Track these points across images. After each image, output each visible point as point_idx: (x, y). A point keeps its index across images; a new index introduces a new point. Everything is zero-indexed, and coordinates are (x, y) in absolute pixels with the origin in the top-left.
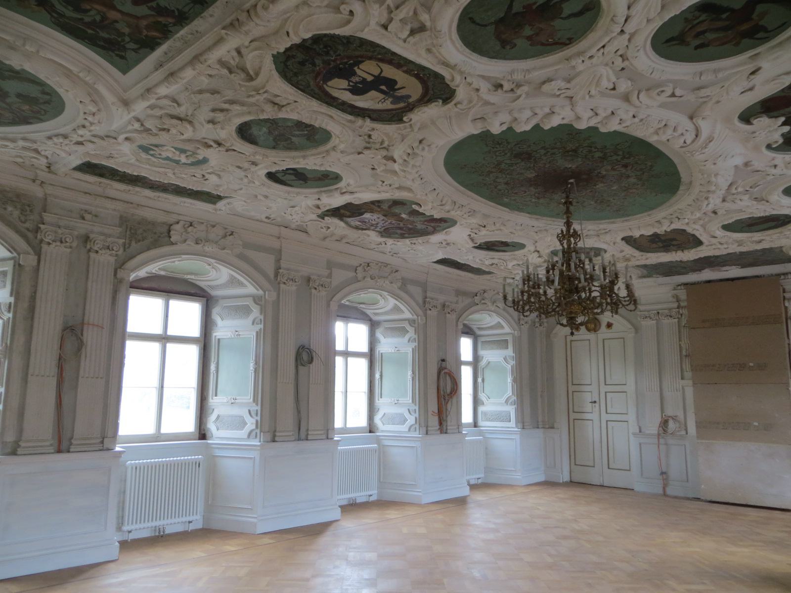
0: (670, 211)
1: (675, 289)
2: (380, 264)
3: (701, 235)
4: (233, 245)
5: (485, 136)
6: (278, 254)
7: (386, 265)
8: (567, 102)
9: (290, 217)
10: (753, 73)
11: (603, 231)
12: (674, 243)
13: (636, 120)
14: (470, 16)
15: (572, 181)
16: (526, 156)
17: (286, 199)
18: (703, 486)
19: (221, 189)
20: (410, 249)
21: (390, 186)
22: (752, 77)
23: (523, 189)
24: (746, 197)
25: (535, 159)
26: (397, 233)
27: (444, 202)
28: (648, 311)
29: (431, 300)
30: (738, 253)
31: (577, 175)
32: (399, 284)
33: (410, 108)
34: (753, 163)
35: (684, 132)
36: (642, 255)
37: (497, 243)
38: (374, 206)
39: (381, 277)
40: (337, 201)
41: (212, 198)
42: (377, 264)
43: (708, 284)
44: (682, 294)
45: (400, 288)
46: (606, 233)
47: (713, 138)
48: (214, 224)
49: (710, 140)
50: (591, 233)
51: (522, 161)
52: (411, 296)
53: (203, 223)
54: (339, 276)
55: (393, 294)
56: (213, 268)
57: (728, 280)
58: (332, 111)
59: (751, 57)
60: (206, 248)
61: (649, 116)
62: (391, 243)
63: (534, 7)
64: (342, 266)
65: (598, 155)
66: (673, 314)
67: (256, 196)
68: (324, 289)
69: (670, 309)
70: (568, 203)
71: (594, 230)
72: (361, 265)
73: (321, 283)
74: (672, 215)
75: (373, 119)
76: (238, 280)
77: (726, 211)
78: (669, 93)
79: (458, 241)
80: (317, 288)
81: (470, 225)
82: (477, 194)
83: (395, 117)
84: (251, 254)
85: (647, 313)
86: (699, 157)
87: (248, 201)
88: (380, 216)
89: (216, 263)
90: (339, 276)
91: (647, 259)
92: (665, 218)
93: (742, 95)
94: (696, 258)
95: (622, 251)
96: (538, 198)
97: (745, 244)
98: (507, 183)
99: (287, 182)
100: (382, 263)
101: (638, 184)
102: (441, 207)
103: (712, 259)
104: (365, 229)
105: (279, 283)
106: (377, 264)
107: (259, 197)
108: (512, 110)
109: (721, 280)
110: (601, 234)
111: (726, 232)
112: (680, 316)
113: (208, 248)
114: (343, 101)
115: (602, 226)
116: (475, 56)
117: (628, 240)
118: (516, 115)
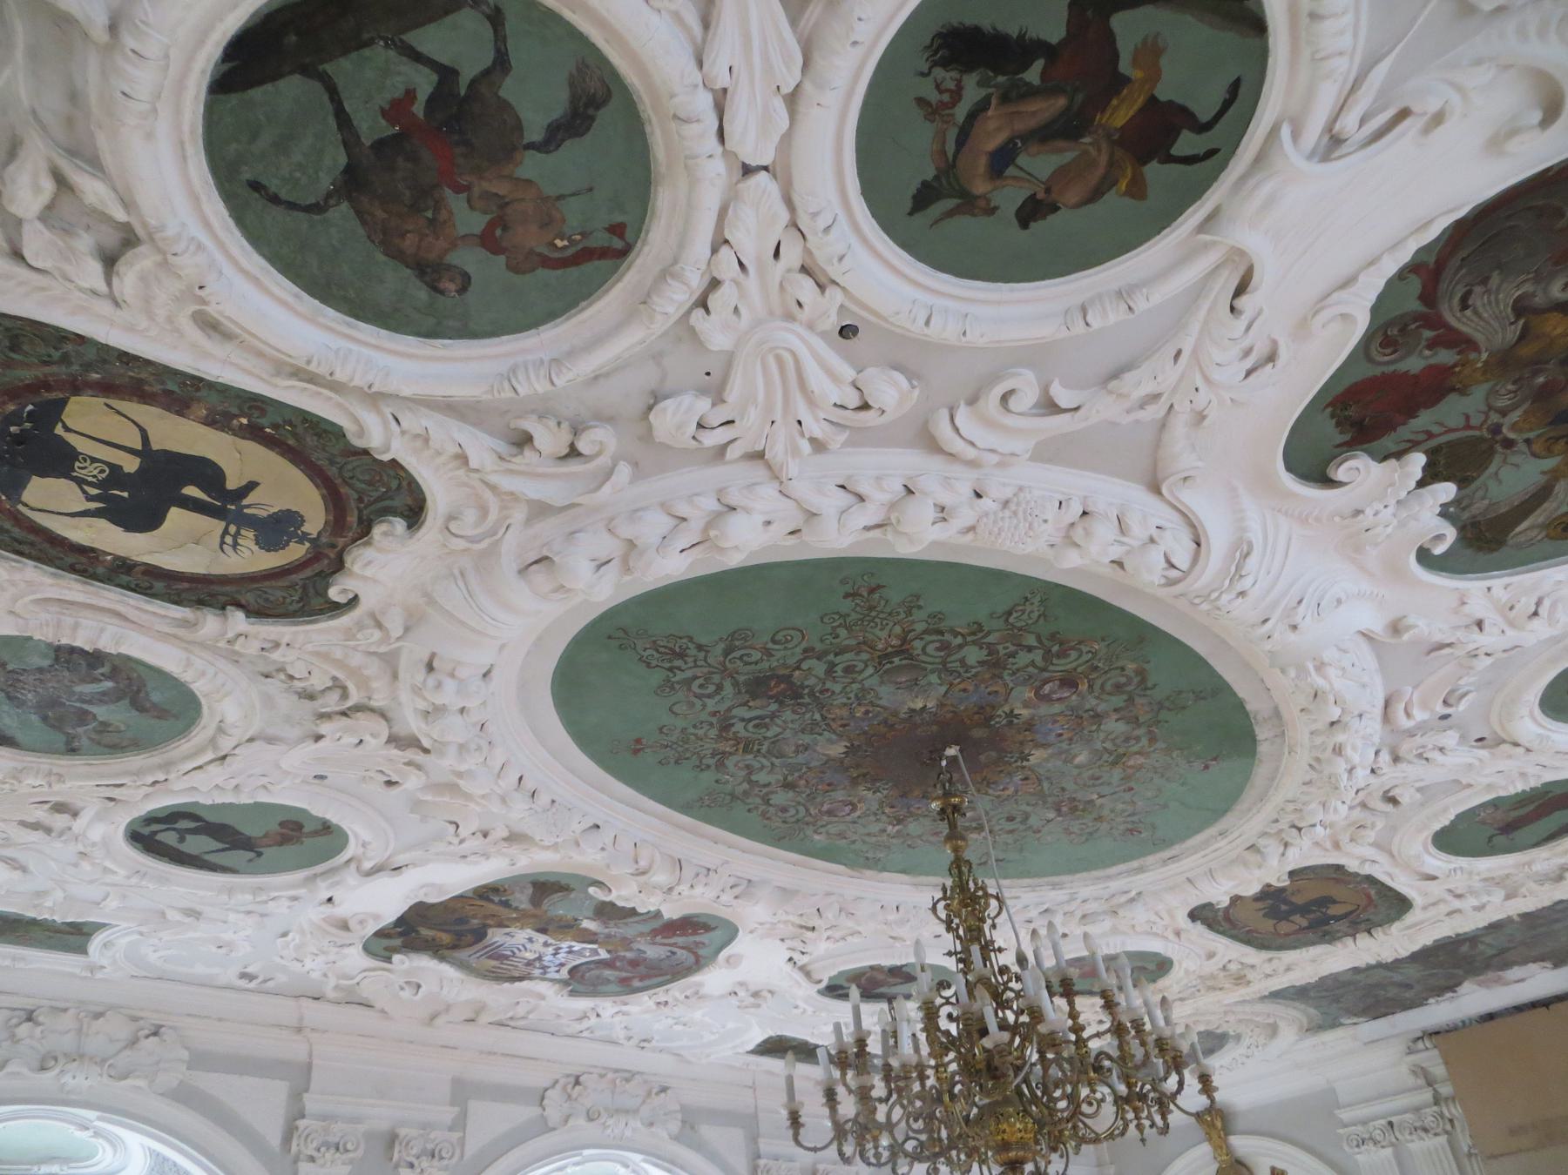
0: (1268, 810)
1: (1410, 1052)
2: (610, 1075)
3: (1390, 875)
4: (158, 1063)
6: (300, 1076)
7: (629, 1076)
8: (757, 471)
9: (297, 966)
10: (1240, 291)
11: (1124, 899)
12: (1334, 910)
13: (986, 503)
14: (247, 174)
15: (952, 751)
17: (249, 912)
19: (49, 904)
20: (670, 1021)
21: (485, 836)
22: (1243, 302)
23: (840, 795)
24: (1450, 739)
25: (812, 694)
26: (608, 981)
27: (643, 863)
28: (1364, 1123)
29: (771, 1163)
30: (1516, 918)
31: (952, 728)
32: (675, 1126)
34: (1411, 620)
35: (1155, 532)
36: (1270, 960)
37: (881, 977)
39: (617, 1111)
41: (73, 936)
42: (602, 1076)
43: (1488, 1025)
44: (1432, 1060)
45: (676, 1138)
46: (1132, 900)
47: (1250, 545)
48: (99, 1009)
49: (1242, 552)
50: (1093, 907)
51: (781, 703)
52: (713, 1157)
53: (65, 1010)
54: (490, 1120)
55: (659, 1157)
56: (97, 1134)
57: (1534, 1005)
58: (106, 593)
59: (1202, 228)
60: (67, 1079)
61: (1021, 489)
62: (608, 1010)
63: (418, 109)
64: (504, 1093)
65: (973, 655)
66: (1429, 1121)
67: (163, 914)
68: (435, 1162)
69: (1417, 1110)
70: (950, 813)
71: (1096, 899)
72: (556, 1082)
73: (430, 1146)
74: (1277, 821)
75: (258, 612)
76: (175, 1165)
77: (1419, 790)
78: (1027, 397)
80: (416, 1163)
84: (213, 1083)
85: (1360, 1128)
86: (1243, 610)
87: (143, 929)
88: (529, 932)
89: (99, 1119)
90: (490, 1120)
91: (1288, 969)
92: (1264, 834)
93: (1251, 378)
94: (1416, 947)
95: (1211, 956)
96: (899, 822)
97: (1523, 890)
98: (788, 786)
99: (207, 857)
100: (616, 1071)
101: (1138, 739)
102: (642, 879)
103: (1465, 948)
104: (520, 979)
105: (296, 1161)
106: (602, 1076)
107: (173, 915)
108: (612, 519)
109: (1519, 1009)
110: (1121, 906)
111: (1452, 858)
112: (1448, 1127)
113: (78, 1079)
114: (117, 558)
115: (1114, 885)
116: (367, 331)
117: (1202, 915)
118: (626, 531)
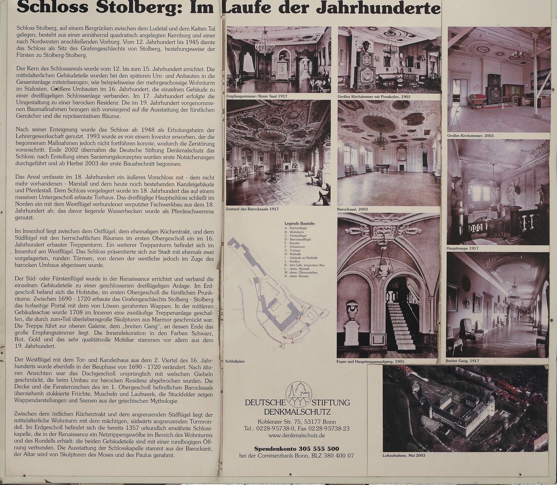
5: (369, 116)
16: (375, 121)
18: (528, 405)
33: (357, 109)
38: (351, 126)
40: (344, 124)
79: (365, 134)
81: (367, 131)
82: (546, 407)
83: (355, 110)
